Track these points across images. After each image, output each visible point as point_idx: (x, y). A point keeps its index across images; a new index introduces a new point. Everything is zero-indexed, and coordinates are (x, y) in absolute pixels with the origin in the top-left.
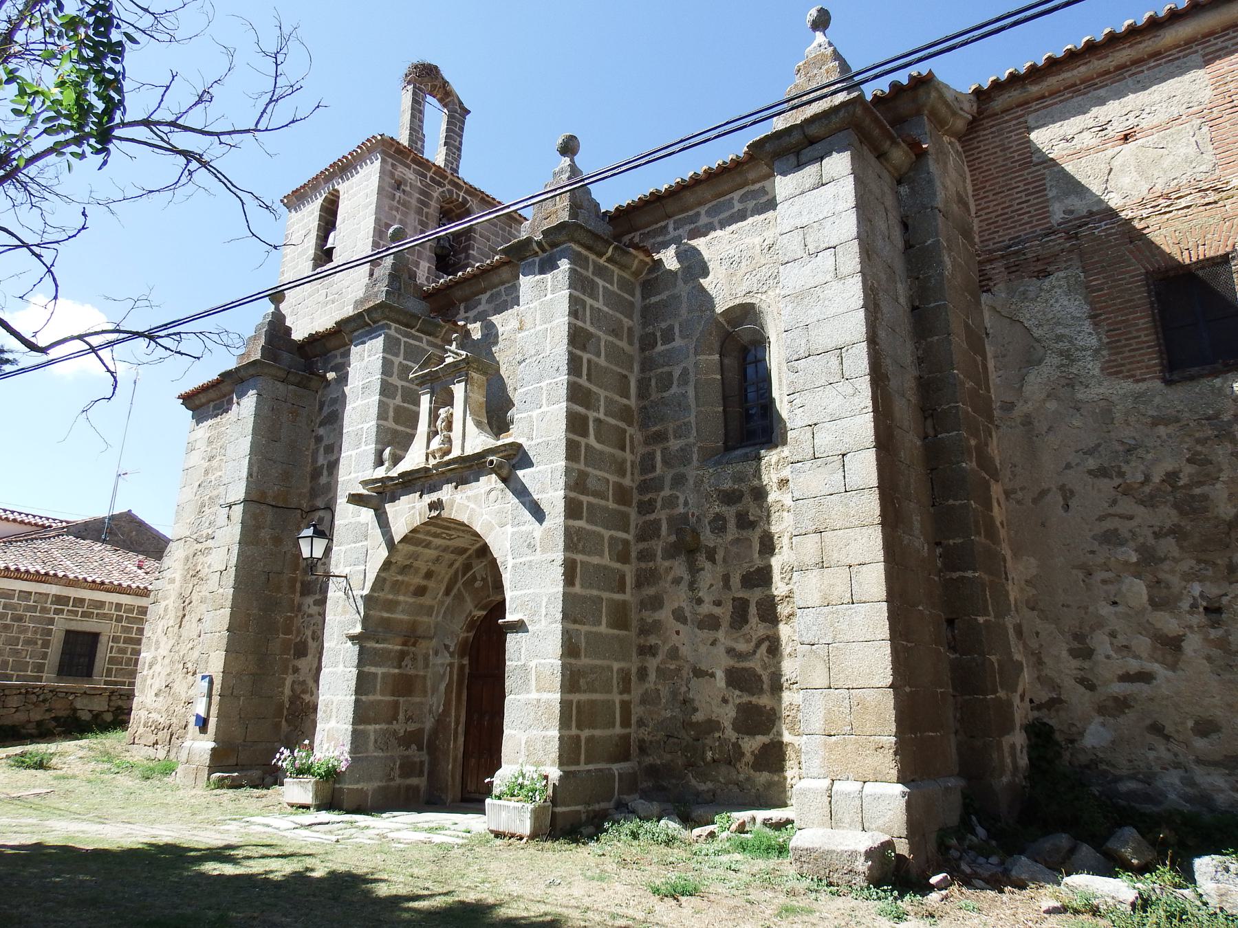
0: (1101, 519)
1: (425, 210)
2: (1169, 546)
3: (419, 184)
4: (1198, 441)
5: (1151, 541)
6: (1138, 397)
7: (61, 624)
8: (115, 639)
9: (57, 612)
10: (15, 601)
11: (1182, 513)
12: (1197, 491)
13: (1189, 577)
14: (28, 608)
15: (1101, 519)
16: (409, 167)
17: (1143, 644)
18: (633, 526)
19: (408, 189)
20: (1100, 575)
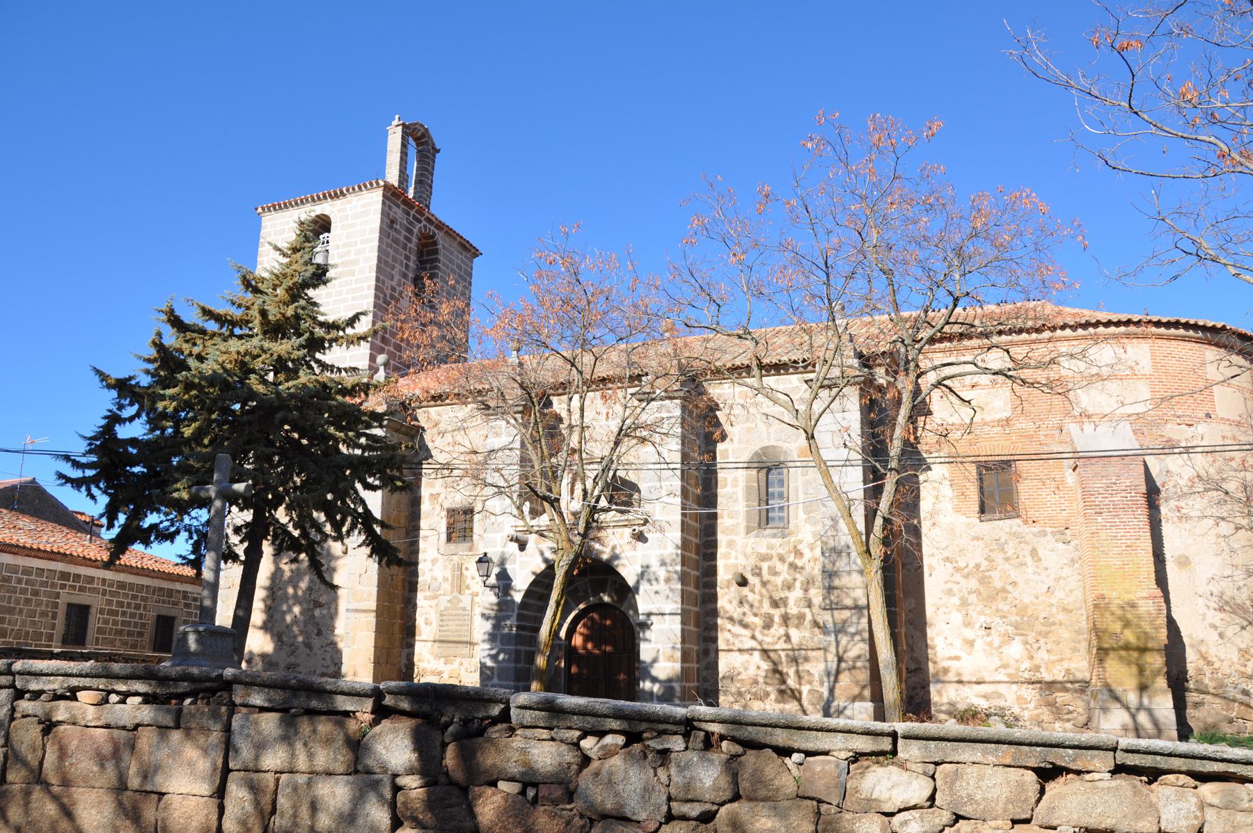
0: (946, 582)
1: (409, 245)
2: (973, 598)
3: (405, 222)
4: (990, 550)
5: (966, 595)
6: (968, 525)
7: (66, 597)
8: (102, 611)
9: (63, 587)
10: (33, 577)
11: (981, 583)
12: (987, 574)
13: (982, 613)
14: (45, 584)
15: (946, 582)
16: (398, 206)
17: (958, 643)
18: (700, 568)
19: (398, 227)
20: (942, 609)
